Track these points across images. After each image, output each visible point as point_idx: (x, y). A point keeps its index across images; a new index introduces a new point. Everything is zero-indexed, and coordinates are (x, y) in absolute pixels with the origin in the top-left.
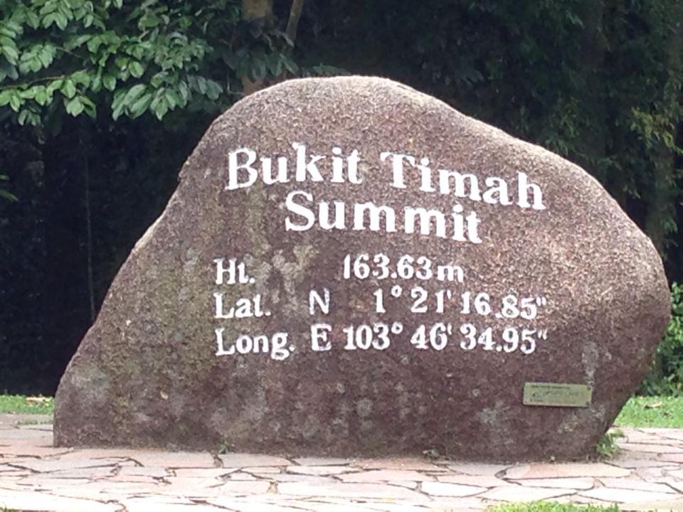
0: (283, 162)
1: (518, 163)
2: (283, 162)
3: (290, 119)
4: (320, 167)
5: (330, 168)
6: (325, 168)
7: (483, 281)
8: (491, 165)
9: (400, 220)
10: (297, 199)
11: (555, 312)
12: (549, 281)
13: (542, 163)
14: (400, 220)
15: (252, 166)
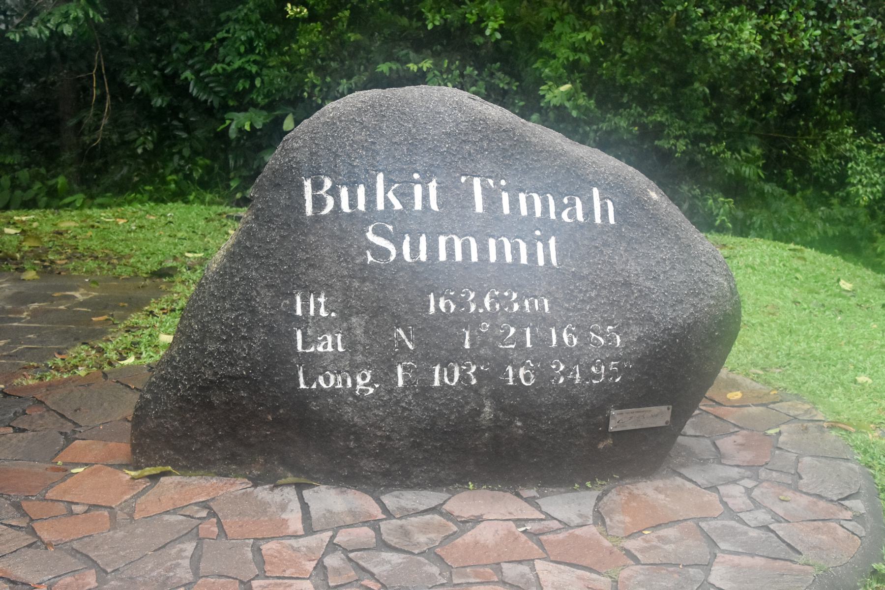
0: (361, 190)
1: (591, 177)
2: (361, 190)
3: (366, 140)
4: (399, 194)
5: (411, 195)
6: (405, 196)
7: (568, 309)
8: (571, 182)
9: (483, 250)
10: (380, 232)
11: (639, 338)
12: (631, 305)
13: (611, 174)
14: (483, 250)
15: (327, 192)
